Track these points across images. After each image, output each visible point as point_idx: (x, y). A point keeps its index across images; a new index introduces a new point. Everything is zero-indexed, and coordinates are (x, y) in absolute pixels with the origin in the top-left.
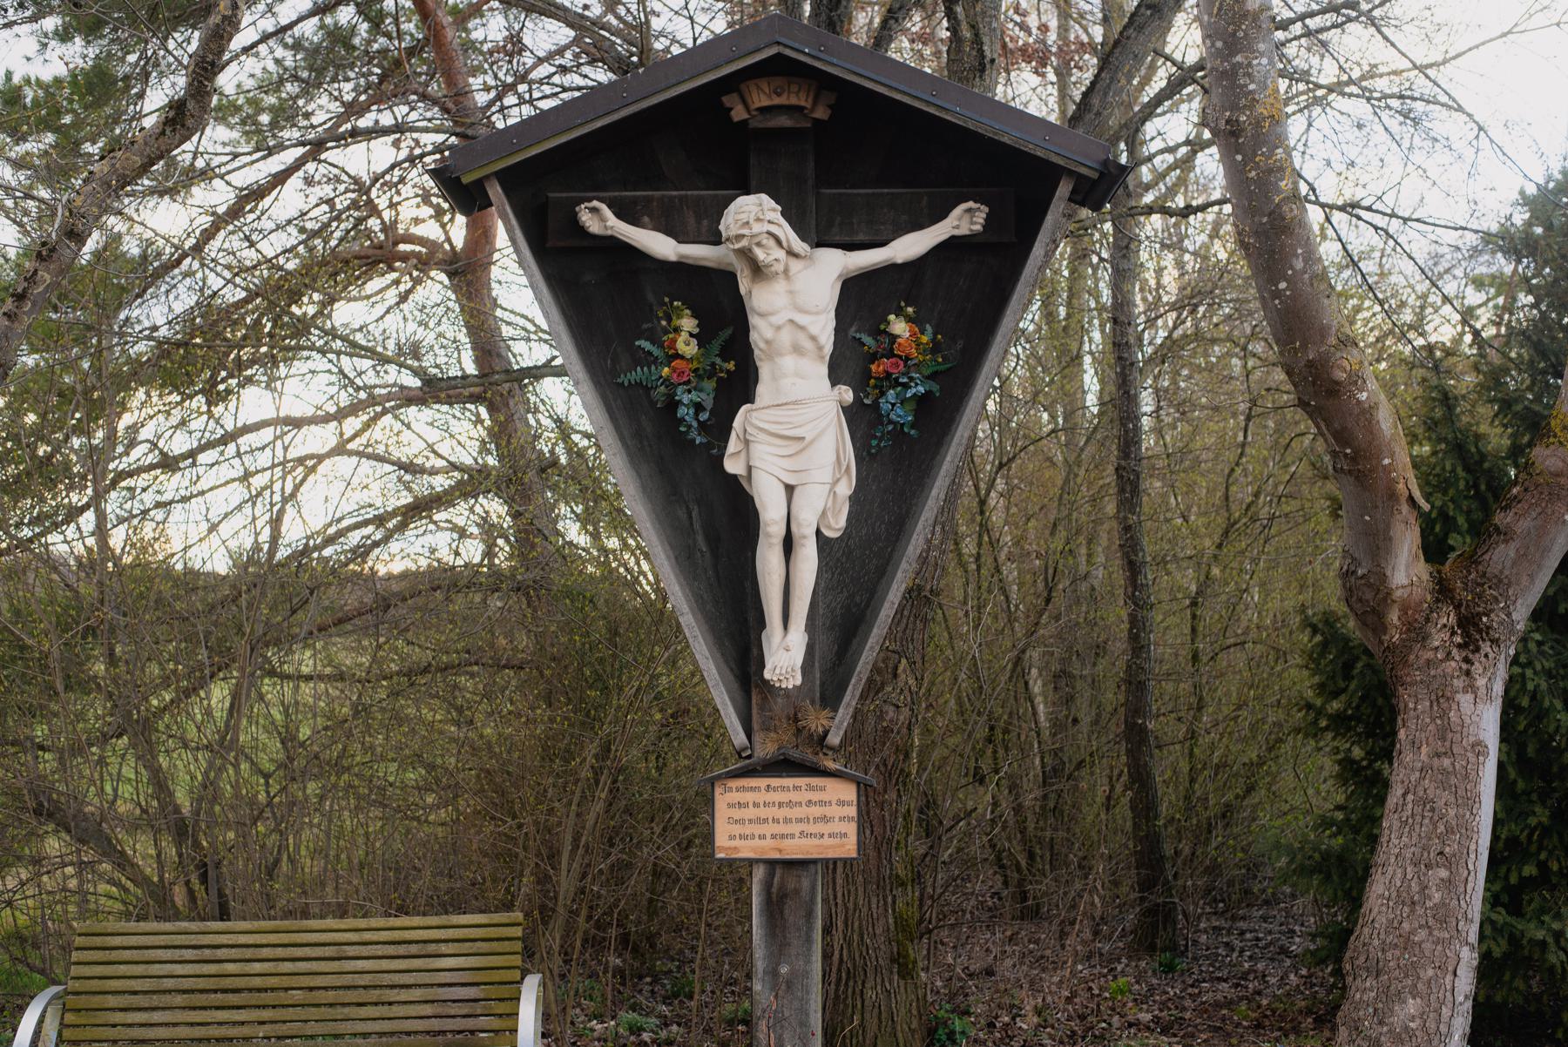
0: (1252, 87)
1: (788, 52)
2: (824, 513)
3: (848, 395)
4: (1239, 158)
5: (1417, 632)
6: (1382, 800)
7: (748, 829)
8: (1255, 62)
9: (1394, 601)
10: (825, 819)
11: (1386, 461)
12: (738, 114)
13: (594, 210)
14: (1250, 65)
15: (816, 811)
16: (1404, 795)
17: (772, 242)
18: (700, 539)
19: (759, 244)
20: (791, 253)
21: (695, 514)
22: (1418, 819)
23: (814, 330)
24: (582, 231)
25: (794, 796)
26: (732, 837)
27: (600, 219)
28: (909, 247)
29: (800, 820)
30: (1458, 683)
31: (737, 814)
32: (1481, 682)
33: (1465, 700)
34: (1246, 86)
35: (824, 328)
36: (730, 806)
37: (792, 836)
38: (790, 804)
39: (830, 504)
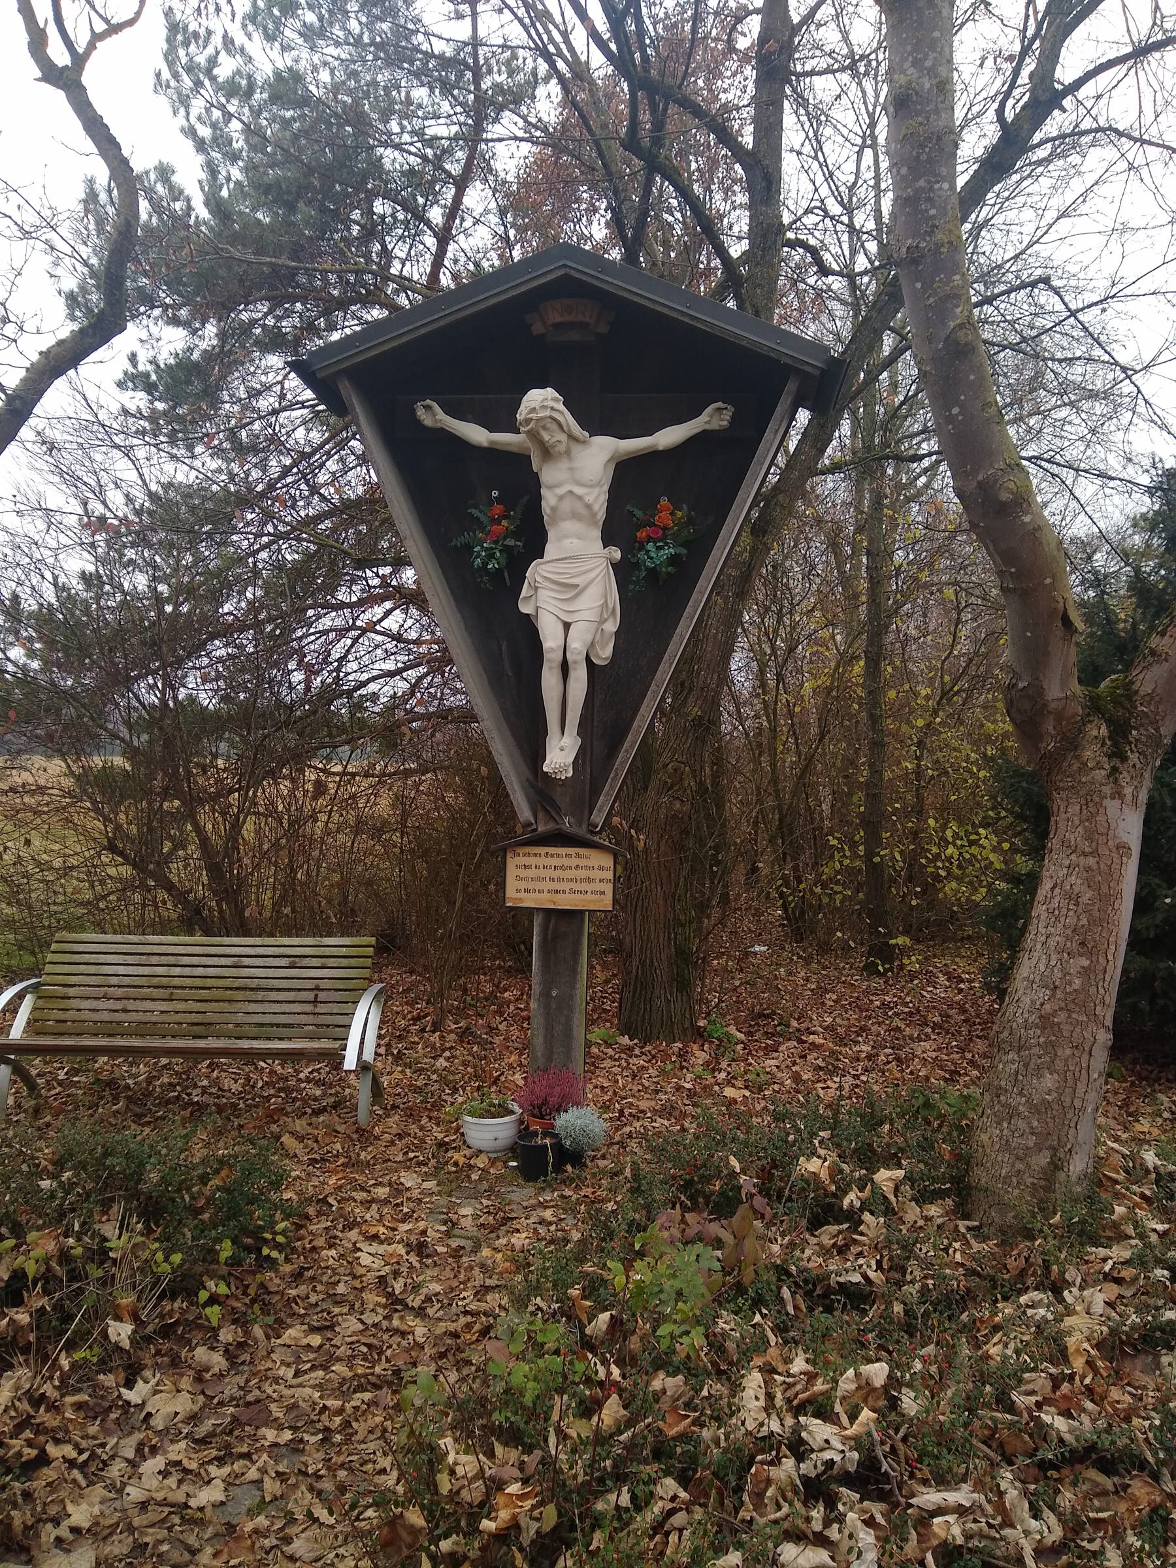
0: (933, 212)
1: (573, 273)
2: (592, 644)
3: (617, 554)
4: (919, 285)
5: (1071, 743)
6: (1033, 892)
7: (531, 885)
8: (937, 186)
9: (1050, 713)
10: (589, 880)
11: (1048, 581)
12: (538, 329)
13: (428, 408)
14: (931, 189)
15: (583, 874)
16: (1052, 889)
17: (554, 426)
18: (507, 666)
19: (544, 428)
20: (572, 437)
21: (504, 647)
22: (1064, 911)
23: (590, 499)
24: (418, 423)
25: (566, 862)
26: (518, 891)
27: (432, 415)
28: (669, 437)
29: (570, 880)
30: (1107, 790)
31: (523, 873)
32: (1128, 791)
33: (1112, 806)
34: (927, 211)
35: (598, 499)
36: (518, 867)
37: (564, 892)
38: (563, 868)
39: (598, 637)
